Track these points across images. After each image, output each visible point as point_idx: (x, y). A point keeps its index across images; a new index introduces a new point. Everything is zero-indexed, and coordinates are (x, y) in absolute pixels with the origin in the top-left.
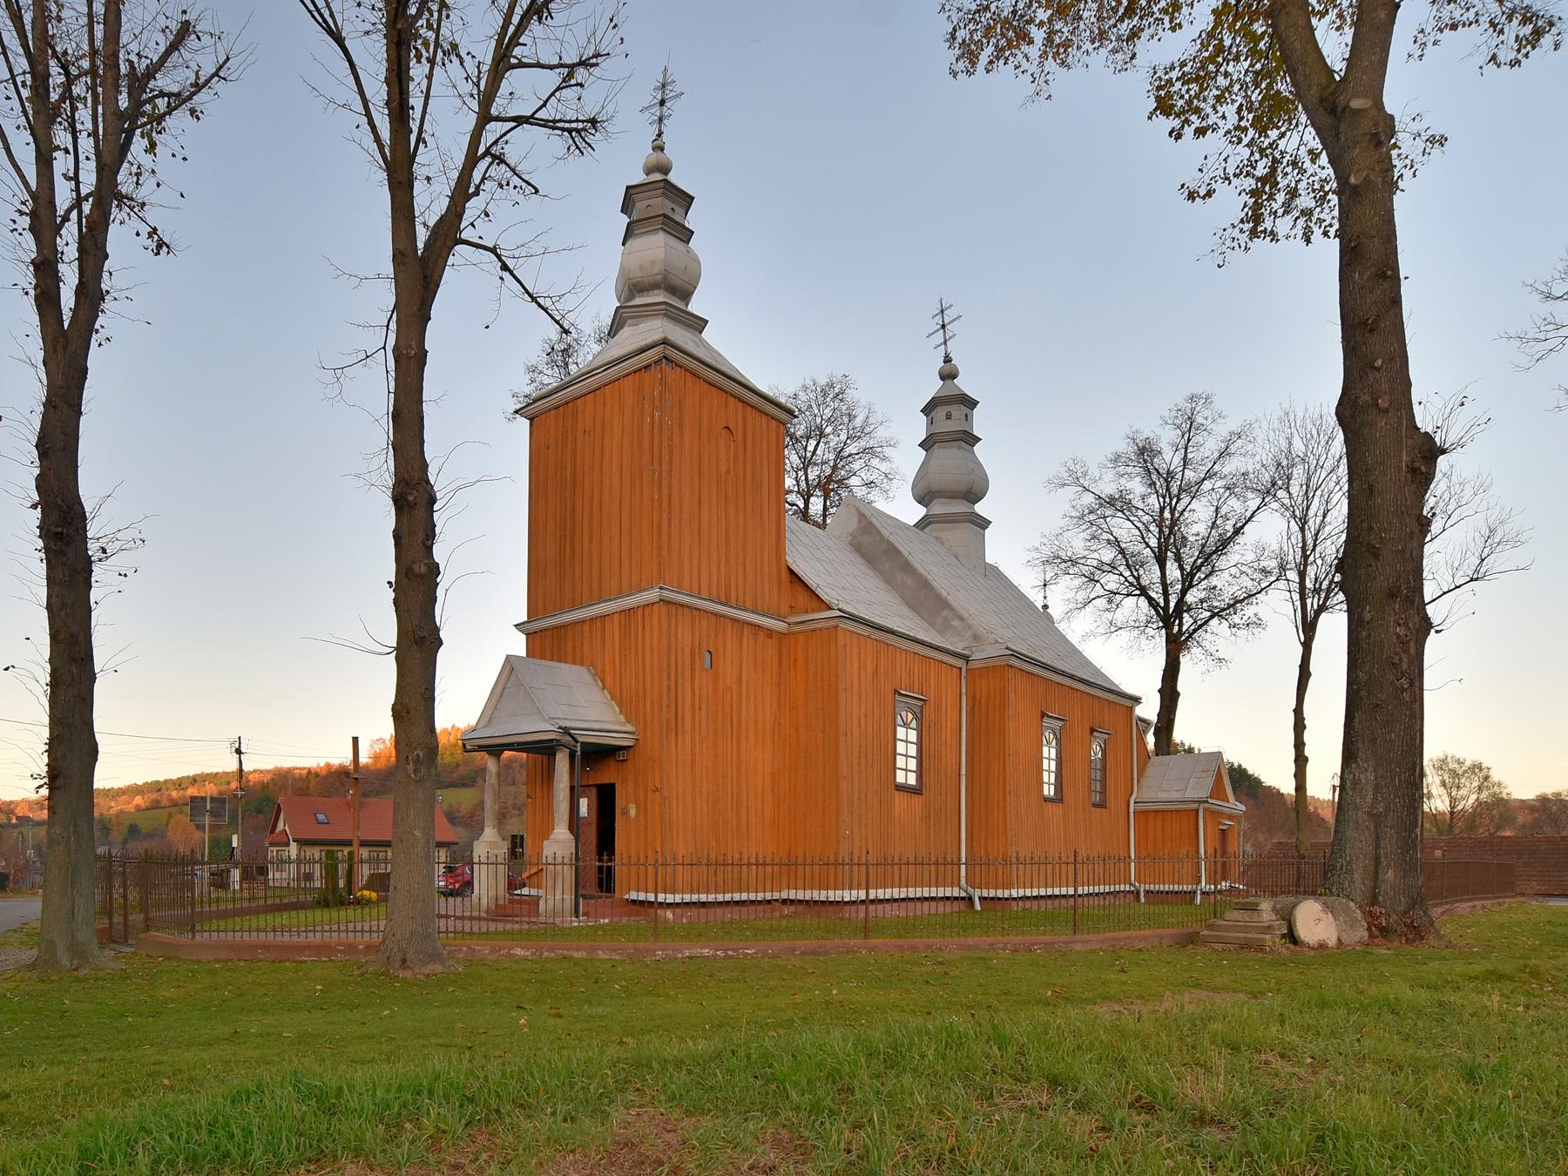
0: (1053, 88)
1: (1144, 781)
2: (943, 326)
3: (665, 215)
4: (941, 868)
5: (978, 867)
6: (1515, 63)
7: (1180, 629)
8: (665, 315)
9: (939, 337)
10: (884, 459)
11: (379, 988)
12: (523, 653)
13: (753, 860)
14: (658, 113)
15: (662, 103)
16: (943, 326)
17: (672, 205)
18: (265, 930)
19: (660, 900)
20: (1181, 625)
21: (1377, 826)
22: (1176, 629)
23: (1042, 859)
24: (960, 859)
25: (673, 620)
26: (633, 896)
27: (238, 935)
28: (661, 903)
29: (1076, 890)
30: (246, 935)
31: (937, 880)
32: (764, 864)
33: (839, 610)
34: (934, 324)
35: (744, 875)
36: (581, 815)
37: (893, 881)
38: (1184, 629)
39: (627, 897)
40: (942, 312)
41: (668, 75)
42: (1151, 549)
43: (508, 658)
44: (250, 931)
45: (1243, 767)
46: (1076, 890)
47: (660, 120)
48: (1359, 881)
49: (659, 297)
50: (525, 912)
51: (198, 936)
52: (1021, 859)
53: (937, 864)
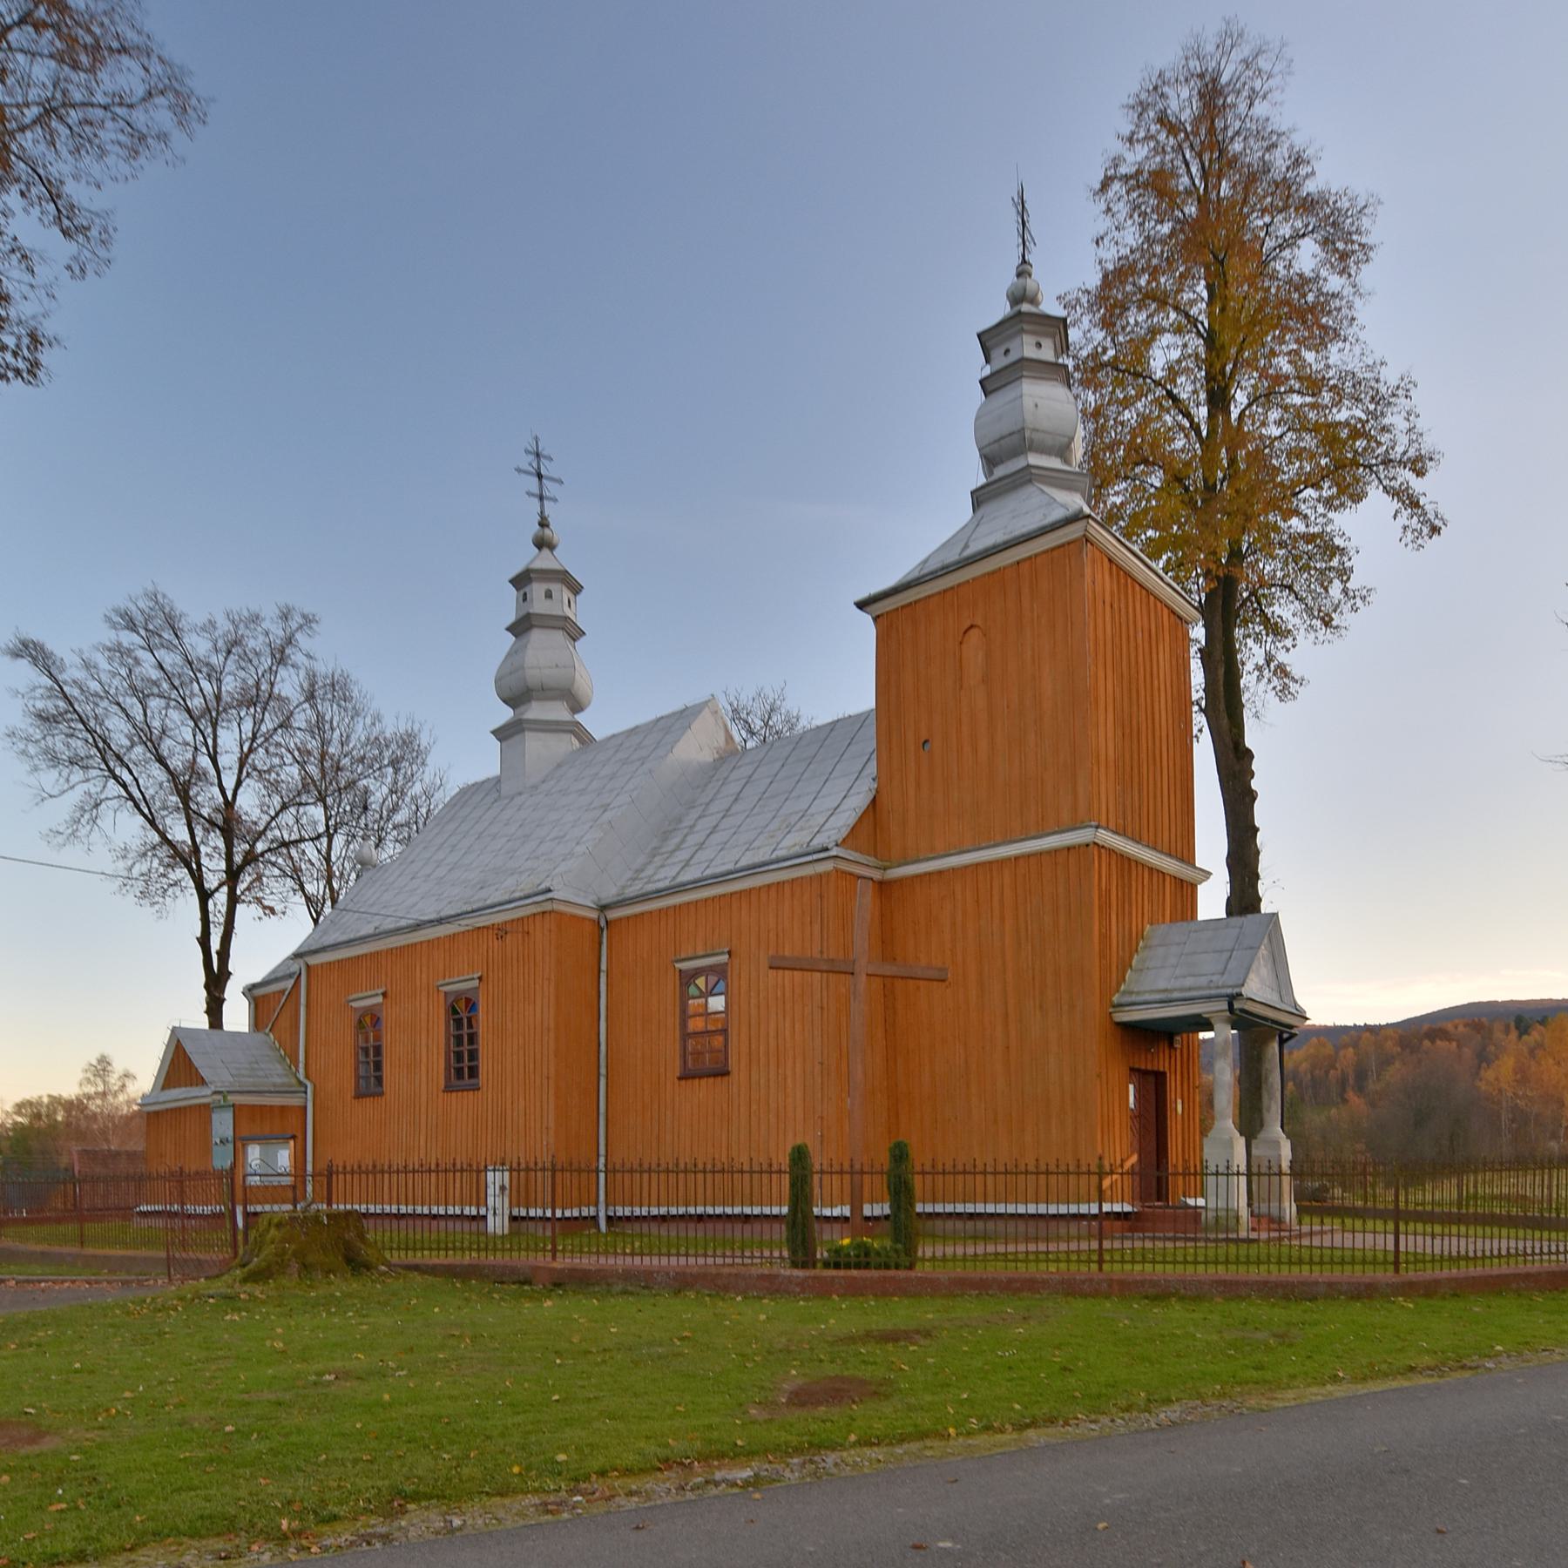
0: (1296, 672)
4: (990, 1178)
5: (386, 1176)
6: (1294, 646)
12: (207, 1026)
13: (709, 1167)
18: (1216, 1263)
23: (765, 1167)
24: (305, 1170)
29: (554, 1213)
30: (1285, 1268)
31: (391, 1199)
32: (1048, 1173)
37: (391, 1199)
43: (174, 1030)
44: (1279, 1262)
45: (55, 1094)
46: (554, 1213)
50: (1084, 1232)
51: (1106, 1267)
52: (363, 1168)
53: (528, 1169)
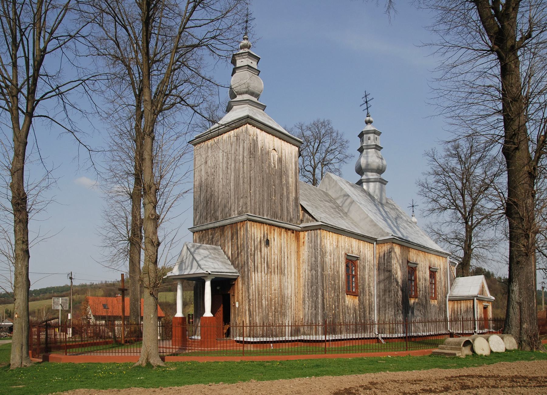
1: (2, 312)
2: (366, 102)
3: (248, 65)
5: (421, 324)
7: (472, 223)
8: (249, 104)
9: (365, 106)
10: (448, 150)
11: (372, 365)
14: (248, 24)
15: (247, 22)
16: (366, 102)
17: (251, 61)
19: (245, 340)
20: (472, 221)
21: (520, 307)
22: (470, 223)
25: (253, 227)
26: (238, 339)
27: (135, 354)
28: (245, 341)
33: (321, 222)
34: (363, 101)
35: (284, 330)
36: (537, 289)
38: (473, 223)
39: (235, 339)
40: (366, 96)
41: (249, 11)
42: (459, 190)
47: (246, 28)
48: (515, 330)
49: (246, 97)
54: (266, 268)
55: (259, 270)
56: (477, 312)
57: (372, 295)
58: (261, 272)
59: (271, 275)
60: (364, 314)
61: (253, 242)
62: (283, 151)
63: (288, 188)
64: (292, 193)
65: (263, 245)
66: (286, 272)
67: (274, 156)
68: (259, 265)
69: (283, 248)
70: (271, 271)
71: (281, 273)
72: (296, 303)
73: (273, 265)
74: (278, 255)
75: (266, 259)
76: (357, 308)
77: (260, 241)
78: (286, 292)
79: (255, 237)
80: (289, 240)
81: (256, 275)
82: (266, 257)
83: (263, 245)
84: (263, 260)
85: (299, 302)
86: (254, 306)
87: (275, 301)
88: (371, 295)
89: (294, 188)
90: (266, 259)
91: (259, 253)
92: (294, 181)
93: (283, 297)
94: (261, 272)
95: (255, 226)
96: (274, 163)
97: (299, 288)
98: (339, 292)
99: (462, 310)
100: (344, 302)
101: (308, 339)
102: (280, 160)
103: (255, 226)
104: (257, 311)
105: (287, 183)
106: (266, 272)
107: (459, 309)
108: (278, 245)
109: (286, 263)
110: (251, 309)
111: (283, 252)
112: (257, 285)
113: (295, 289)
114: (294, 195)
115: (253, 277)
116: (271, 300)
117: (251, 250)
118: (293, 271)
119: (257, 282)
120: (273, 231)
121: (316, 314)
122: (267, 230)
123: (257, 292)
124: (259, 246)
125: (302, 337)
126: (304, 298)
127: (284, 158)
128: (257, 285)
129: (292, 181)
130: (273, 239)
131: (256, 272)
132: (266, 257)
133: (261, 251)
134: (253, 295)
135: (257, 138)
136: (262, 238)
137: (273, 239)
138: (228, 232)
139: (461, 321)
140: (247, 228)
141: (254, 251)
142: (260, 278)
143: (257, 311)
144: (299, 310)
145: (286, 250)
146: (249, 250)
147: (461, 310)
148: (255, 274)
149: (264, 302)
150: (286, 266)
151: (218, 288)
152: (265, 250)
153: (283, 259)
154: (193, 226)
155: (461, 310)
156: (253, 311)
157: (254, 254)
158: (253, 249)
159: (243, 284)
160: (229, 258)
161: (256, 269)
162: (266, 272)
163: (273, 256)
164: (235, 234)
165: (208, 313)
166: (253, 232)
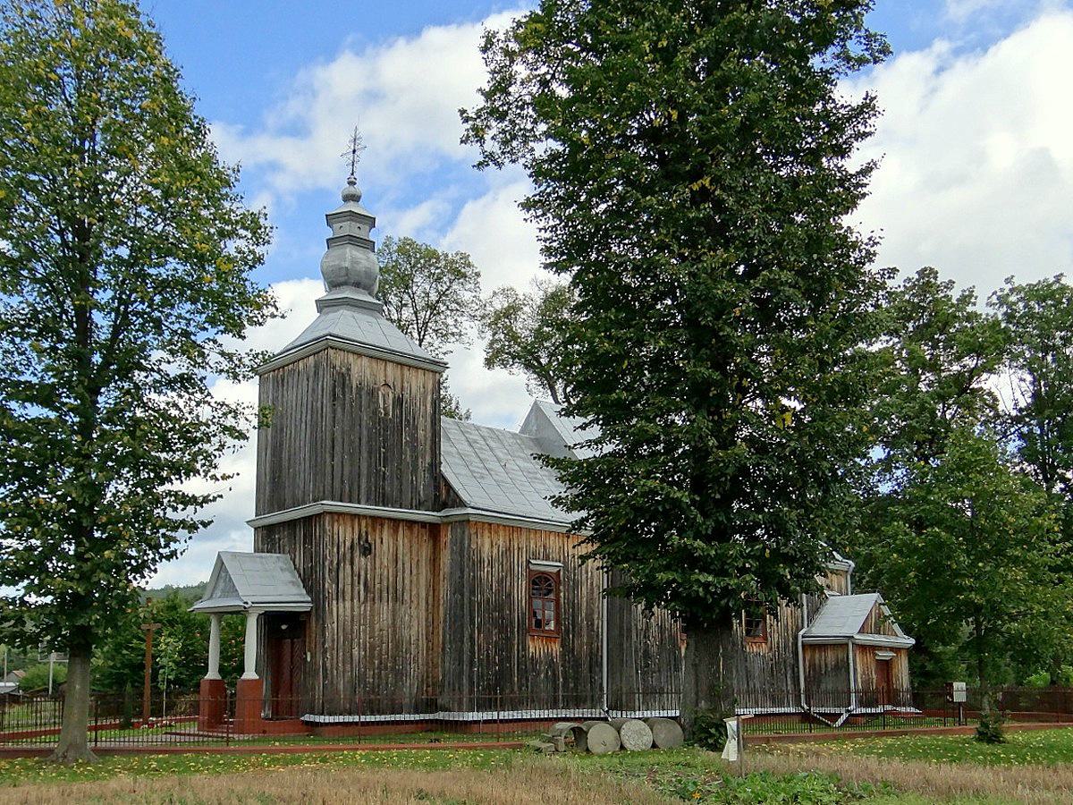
25: (336, 524)
54: (362, 592)
55: (348, 597)
56: (855, 670)
57: (598, 636)
58: (352, 600)
59: (374, 603)
60: (577, 672)
61: (335, 550)
62: (406, 385)
63: (414, 449)
64: (424, 457)
65: (357, 553)
66: (407, 597)
67: (385, 400)
68: (348, 589)
69: (400, 556)
70: (374, 597)
71: (396, 599)
72: (427, 652)
73: (378, 586)
74: (390, 571)
75: (362, 578)
76: (558, 660)
77: (352, 547)
78: (406, 633)
79: (341, 540)
80: (415, 540)
81: (341, 605)
82: (363, 573)
83: (357, 553)
84: (356, 578)
85: (435, 649)
86: (335, 660)
87: (381, 650)
88: (593, 634)
89: (428, 447)
90: (362, 578)
91: (348, 567)
92: (429, 435)
93: (397, 645)
94: (352, 600)
95: (341, 521)
96: (385, 409)
97: (435, 624)
98: (512, 632)
99: (829, 666)
100: (524, 649)
101: (471, 719)
102: (399, 402)
103: (341, 521)
104: (341, 669)
105: (414, 439)
106: (362, 599)
107: (823, 663)
108: (391, 550)
109: (407, 582)
110: (328, 665)
111: (400, 563)
112: (341, 623)
113: (427, 627)
114: (428, 459)
115: (335, 609)
116: (373, 648)
117: (332, 562)
118: (423, 594)
119: (341, 618)
120: (379, 527)
121: (460, 673)
122: (366, 527)
123: (341, 634)
124: (348, 556)
125: (440, 716)
126: (444, 643)
127: (406, 396)
128: (341, 623)
129: (425, 436)
130: (378, 541)
131: (341, 600)
132: (363, 573)
133: (352, 564)
134: (333, 641)
135: (349, 370)
136: (356, 541)
137: (378, 541)
138: (300, 533)
139: (668, 693)
140: (324, 525)
141: (338, 564)
142: (349, 611)
143: (341, 669)
144: (435, 666)
145: (407, 559)
146: (327, 563)
147: (826, 665)
148: (337, 604)
149: (355, 652)
150: (407, 588)
151: (284, 627)
152: (361, 561)
153: (400, 574)
154: (253, 517)
155: (826, 665)
156: (332, 669)
157: (338, 569)
158: (335, 562)
159: (317, 620)
160: (300, 575)
161: (340, 595)
162: (362, 599)
163: (378, 571)
164: (308, 538)
165: (250, 674)
166: (336, 531)
